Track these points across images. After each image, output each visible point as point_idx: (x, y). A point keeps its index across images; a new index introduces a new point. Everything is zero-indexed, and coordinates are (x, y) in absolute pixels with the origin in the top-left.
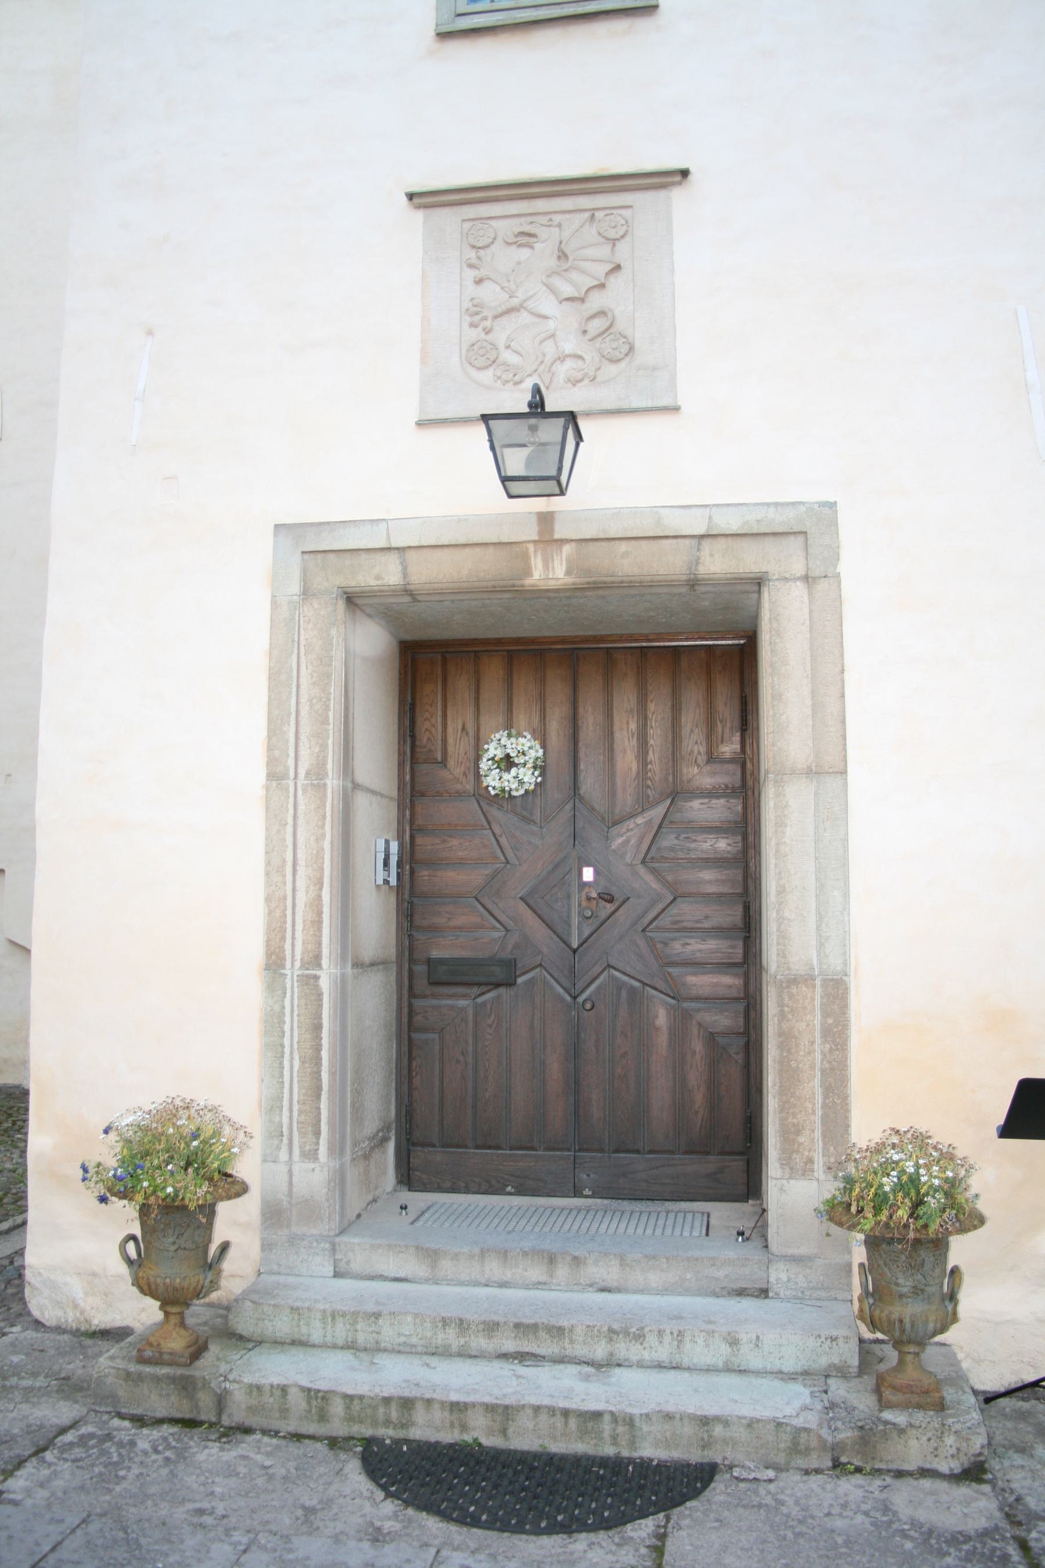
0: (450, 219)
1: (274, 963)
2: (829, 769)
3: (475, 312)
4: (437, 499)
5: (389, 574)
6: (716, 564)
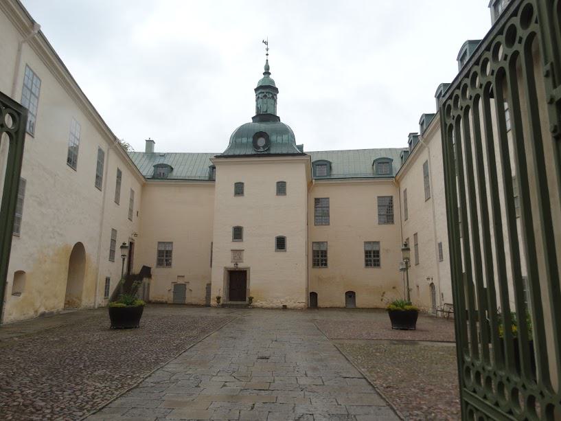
4: (231, 266)
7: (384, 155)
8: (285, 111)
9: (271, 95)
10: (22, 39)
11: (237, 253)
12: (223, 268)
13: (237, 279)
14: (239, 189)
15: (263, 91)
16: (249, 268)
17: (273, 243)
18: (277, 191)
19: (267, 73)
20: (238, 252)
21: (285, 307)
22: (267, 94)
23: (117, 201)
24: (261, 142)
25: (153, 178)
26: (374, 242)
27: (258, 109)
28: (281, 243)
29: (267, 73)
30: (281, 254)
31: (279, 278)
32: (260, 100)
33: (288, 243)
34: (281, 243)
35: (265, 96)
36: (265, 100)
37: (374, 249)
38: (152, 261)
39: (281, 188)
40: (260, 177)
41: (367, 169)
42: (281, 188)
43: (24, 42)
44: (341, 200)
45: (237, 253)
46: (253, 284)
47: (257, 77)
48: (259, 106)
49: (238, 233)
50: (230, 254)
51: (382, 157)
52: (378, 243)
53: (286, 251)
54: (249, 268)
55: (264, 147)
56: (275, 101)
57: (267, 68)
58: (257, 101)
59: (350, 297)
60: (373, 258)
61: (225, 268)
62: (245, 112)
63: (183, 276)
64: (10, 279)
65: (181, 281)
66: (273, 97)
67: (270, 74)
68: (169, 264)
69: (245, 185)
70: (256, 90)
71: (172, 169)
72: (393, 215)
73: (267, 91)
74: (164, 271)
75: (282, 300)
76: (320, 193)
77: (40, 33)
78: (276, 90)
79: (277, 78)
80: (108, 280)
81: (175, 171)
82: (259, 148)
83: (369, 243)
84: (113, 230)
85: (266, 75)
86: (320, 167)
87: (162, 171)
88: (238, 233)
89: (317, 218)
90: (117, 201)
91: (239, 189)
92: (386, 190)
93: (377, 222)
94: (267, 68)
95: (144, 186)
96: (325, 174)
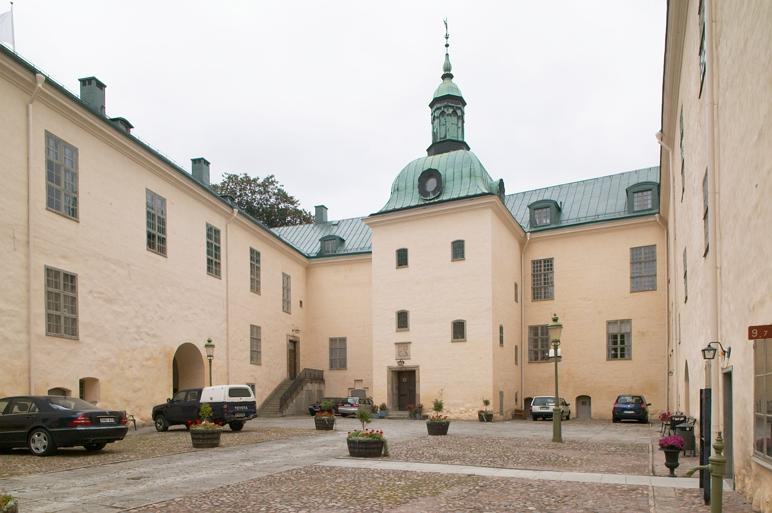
4: (395, 364)
9: (451, 111)
10: (28, 98)
11: (403, 346)
12: (386, 369)
13: (404, 381)
14: (402, 258)
15: (438, 106)
17: (449, 330)
18: (406, 256)
19: (447, 76)
21: (670, 373)
23: (255, 286)
24: (431, 184)
25: (320, 255)
26: (622, 322)
27: (434, 135)
28: (459, 330)
29: (447, 76)
30: (459, 346)
31: (460, 379)
32: (437, 121)
33: (469, 330)
34: (459, 330)
36: (442, 119)
37: (623, 331)
39: (458, 250)
40: (429, 237)
41: (618, 204)
42: (458, 250)
43: (31, 102)
44: (572, 259)
45: (403, 346)
46: (426, 392)
47: (434, 87)
48: (52, 158)
49: (403, 320)
50: (394, 349)
51: (640, 181)
52: (629, 321)
53: (465, 341)
54: (418, 367)
55: (434, 192)
56: (461, 118)
57: (447, 68)
58: (433, 123)
59: (584, 403)
60: (618, 346)
62: (413, 141)
64: (25, 413)
66: (455, 113)
67: (451, 76)
70: (431, 105)
71: (343, 241)
74: (338, 374)
76: (540, 252)
77: (49, 82)
78: (464, 104)
79: (462, 85)
81: (347, 243)
83: (615, 322)
84: (252, 326)
85: (447, 80)
86: (640, 194)
87: (330, 245)
88: (403, 320)
89: (635, 266)
90: (255, 286)
91: (402, 258)
92: (644, 237)
94: (447, 68)
95: (308, 269)
96: (650, 206)
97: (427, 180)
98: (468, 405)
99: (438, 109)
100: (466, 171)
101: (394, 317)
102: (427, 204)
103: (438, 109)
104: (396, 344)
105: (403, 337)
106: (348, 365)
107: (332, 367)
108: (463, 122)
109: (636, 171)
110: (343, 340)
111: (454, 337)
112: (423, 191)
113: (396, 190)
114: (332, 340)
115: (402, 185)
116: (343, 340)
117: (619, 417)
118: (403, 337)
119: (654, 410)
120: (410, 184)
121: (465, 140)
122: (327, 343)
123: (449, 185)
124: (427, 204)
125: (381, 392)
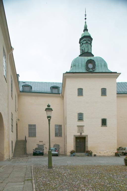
0: (78, 127)
1: (74, 146)
2: (88, 141)
3: (79, 129)
4: (78, 134)
5: (76, 136)
6: (85, 136)
7: (55, 85)
8: (97, 50)
11: (81, 128)
13: (81, 141)
14: (80, 92)
15: (85, 39)
16: (87, 136)
17: (100, 122)
19: (86, 30)
20: (81, 127)
22: (88, 41)
24: (90, 66)
28: (104, 122)
29: (86, 30)
30: (104, 128)
33: (108, 122)
34: (104, 122)
35: (87, 42)
36: (87, 45)
38: (27, 134)
39: (104, 92)
40: (92, 85)
41: (49, 90)
42: (104, 92)
45: (81, 128)
46: (90, 145)
49: (80, 117)
50: (76, 128)
54: (87, 136)
55: (92, 69)
56: (91, 44)
61: (75, 136)
63: (42, 141)
65: (41, 144)
68: (35, 136)
69: (84, 90)
72: (62, 129)
73: (86, 40)
75: (105, 152)
78: (92, 39)
79: (90, 32)
80: (12, 142)
82: (89, 69)
88: (80, 117)
91: (80, 92)
93: (55, 135)
97: (88, 64)
98: (108, 150)
99: (85, 40)
100: (103, 64)
101: (77, 115)
102: (89, 72)
103: (85, 40)
104: (77, 126)
105: (80, 123)
106: (37, 135)
107: (29, 136)
108: (91, 46)
109: (46, 82)
110: (35, 125)
111: (102, 125)
112: (87, 68)
113: (74, 65)
114: (30, 126)
115: (77, 64)
116: (35, 125)
117: (35, 154)
118: (80, 123)
119: (46, 151)
120: (80, 65)
121: (92, 53)
122: (27, 127)
123: (96, 67)
124: (89, 72)
125: (71, 145)
